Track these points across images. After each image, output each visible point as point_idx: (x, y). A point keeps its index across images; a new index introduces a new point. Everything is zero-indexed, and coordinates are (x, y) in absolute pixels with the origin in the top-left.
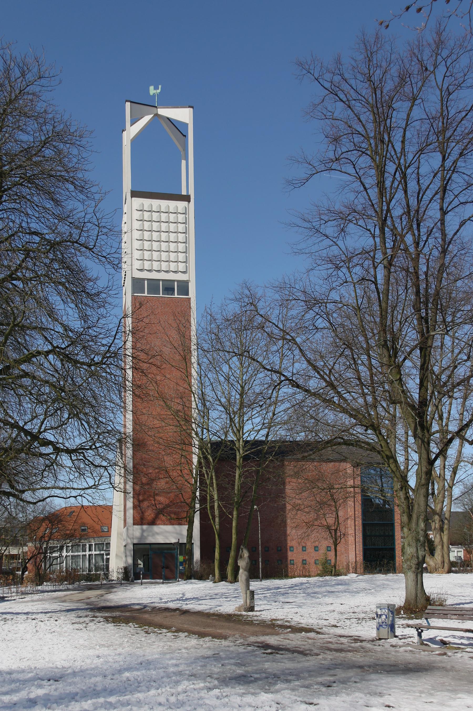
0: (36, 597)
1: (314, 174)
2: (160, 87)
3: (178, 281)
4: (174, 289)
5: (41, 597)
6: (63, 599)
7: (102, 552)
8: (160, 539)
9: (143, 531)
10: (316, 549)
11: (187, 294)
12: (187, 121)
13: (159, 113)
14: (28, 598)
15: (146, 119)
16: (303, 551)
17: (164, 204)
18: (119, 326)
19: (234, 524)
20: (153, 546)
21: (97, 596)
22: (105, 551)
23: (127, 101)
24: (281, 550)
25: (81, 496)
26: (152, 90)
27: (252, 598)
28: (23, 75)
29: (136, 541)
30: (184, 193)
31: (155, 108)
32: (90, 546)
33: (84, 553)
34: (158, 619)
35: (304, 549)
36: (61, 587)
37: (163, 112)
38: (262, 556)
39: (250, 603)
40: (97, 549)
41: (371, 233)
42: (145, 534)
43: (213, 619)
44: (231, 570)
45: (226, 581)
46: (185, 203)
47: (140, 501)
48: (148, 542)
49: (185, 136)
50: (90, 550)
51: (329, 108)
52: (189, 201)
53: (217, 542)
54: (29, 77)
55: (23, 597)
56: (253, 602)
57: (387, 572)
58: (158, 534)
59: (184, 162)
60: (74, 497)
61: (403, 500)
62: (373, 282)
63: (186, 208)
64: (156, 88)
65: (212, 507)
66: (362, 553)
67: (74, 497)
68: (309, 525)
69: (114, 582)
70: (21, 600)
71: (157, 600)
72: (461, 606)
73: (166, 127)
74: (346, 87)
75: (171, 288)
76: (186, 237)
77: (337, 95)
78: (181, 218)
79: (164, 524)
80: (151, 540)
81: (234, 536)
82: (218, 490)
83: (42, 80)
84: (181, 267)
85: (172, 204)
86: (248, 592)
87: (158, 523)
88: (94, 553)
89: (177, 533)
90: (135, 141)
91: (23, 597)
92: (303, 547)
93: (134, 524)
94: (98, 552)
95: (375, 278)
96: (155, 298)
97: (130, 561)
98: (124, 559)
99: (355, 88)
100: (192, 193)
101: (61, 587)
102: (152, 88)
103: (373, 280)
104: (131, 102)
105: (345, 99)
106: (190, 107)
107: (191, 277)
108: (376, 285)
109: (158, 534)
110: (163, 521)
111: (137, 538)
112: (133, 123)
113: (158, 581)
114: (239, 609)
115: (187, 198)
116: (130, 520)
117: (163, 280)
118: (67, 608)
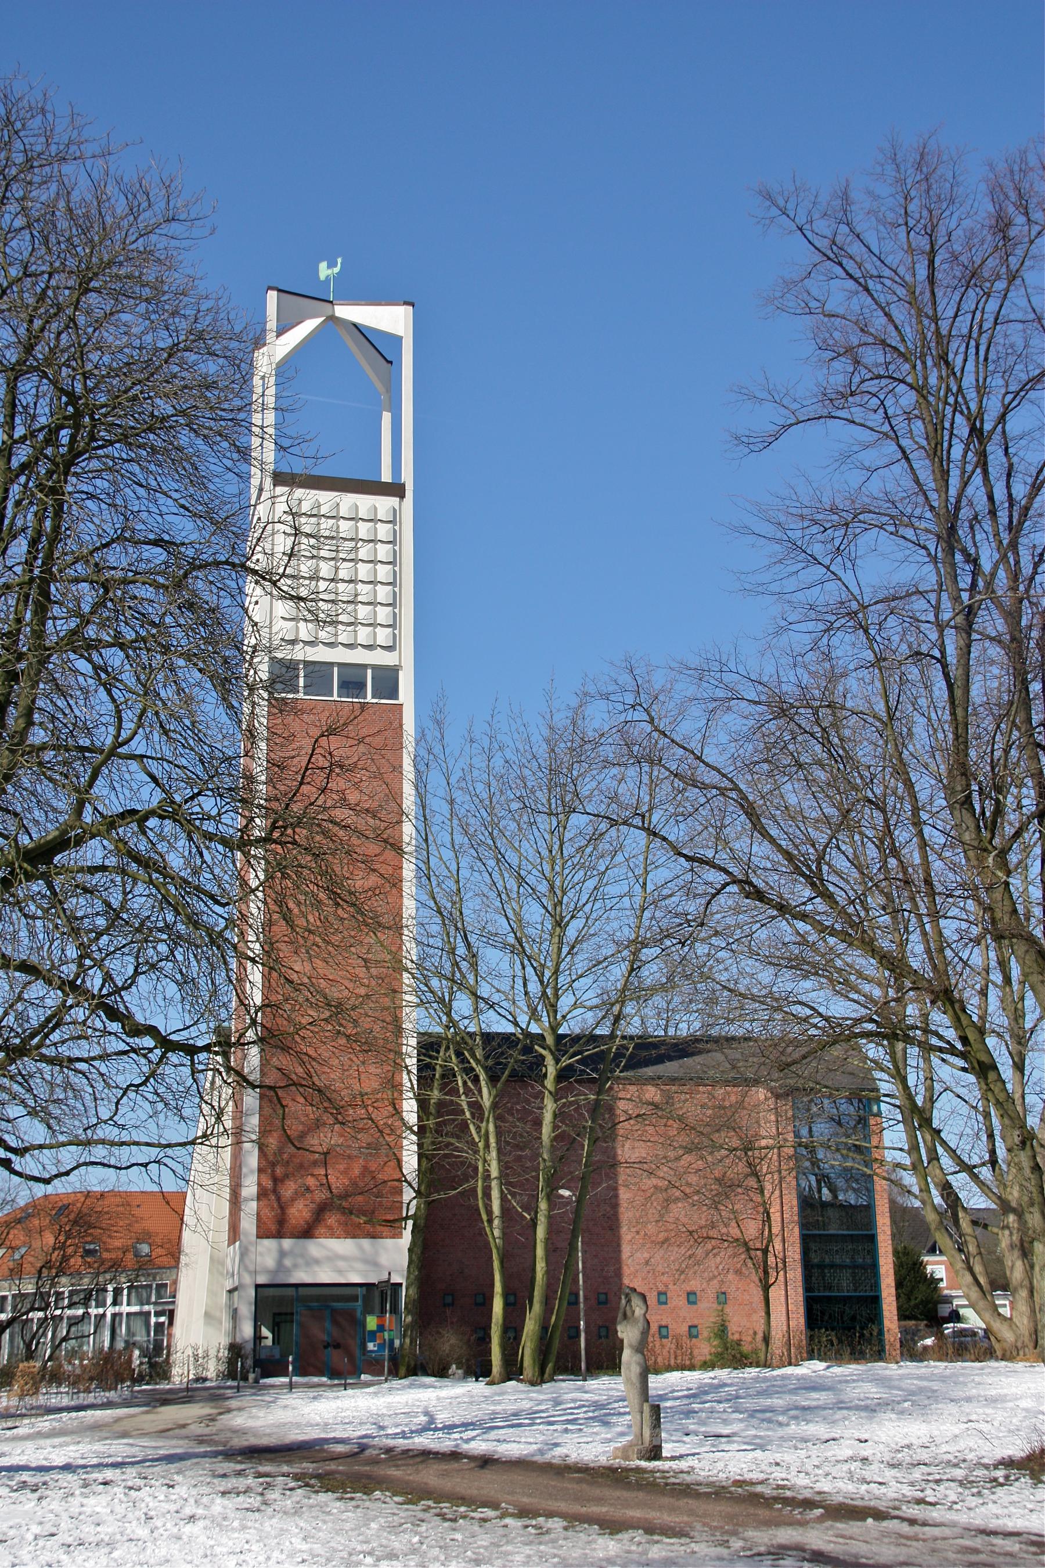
0: (45, 1423)
1: (791, 425)
2: (339, 260)
3: (374, 667)
4: (365, 685)
5: (56, 1424)
6: (118, 1428)
7: (146, 1308)
8: (325, 1276)
9: (282, 1254)
10: (691, 1297)
11: (394, 693)
12: (400, 332)
13: (337, 314)
14: (25, 1427)
15: (309, 326)
16: (660, 1303)
17: (348, 501)
18: (312, 755)
19: (541, 1232)
20: (302, 1291)
21: (201, 1420)
22: (155, 1304)
23: (270, 288)
24: (606, 1302)
25: (158, 1162)
26: (324, 271)
27: (656, 1424)
28: (133, 211)
29: (262, 1280)
30: (386, 477)
31: (329, 305)
32: (117, 1292)
33: (101, 1311)
34: (430, 1476)
35: (663, 1298)
36: (91, 1398)
37: (343, 312)
38: (586, 1315)
39: (652, 1436)
40: (133, 1299)
41: (929, 554)
42: (288, 1262)
43: (580, 1481)
44: (534, 1351)
45: (519, 1380)
46: (394, 501)
47: (275, 1180)
48: (293, 1280)
49: (391, 363)
50: (115, 1303)
51: (815, 292)
52: (402, 496)
53: (497, 1277)
54: (147, 218)
55: (10, 1424)
56: (658, 1435)
57: (858, 1356)
58: (317, 1262)
59: (386, 417)
60: (141, 1165)
61: (1027, 1172)
62: (938, 661)
63: (395, 510)
64: (330, 266)
65: (487, 1195)
66: (802, 1310)
67: (141, 1165)
68: (697, 1237)
69: (208, 1384)
70: (9, 1433)
71: (371, 1430)
72: (119, 1449)
73: (351, 343)
74: (856, 249)
75: (356, 683)
76: (395, 572)
77: (840, 264)
78: (383, 531)
79: (332, 1236)
80: (302, 1276)
81: (540, 1266)
82: (499, 1151)
83: (174, 224)
84: (383, 636)
85: (365, 503)
86: (646, 1407)
87: (317, 1232)
88: (125, 1309)
89: (366, 1261)
90: (285, 369)
91: (10, 1424)
92: (660, 1294)
93: (259, 1236)
94: (135, 1309)
95: (943, 652)
96: (322, 704)
97: (247, 1330)
98: (226, 1324)
99: (877, 253)
100: (407, 477)
101: (91, 1398)
102: (323, 265)
103: (938, 655)
104: (279, 290)
105: (857, 274)
106: (406, 303)
107: (405, 659)
108: (945, 666)
109: (317, 1262)
110: (330, 1228)
111: (269, 1272)
112: (280, 333)
113: (316, 1380)
114: (625, 1452)
115: (396, 490)
116: (248, 1224)
117: (340, 665)
118: (172, 1451)
